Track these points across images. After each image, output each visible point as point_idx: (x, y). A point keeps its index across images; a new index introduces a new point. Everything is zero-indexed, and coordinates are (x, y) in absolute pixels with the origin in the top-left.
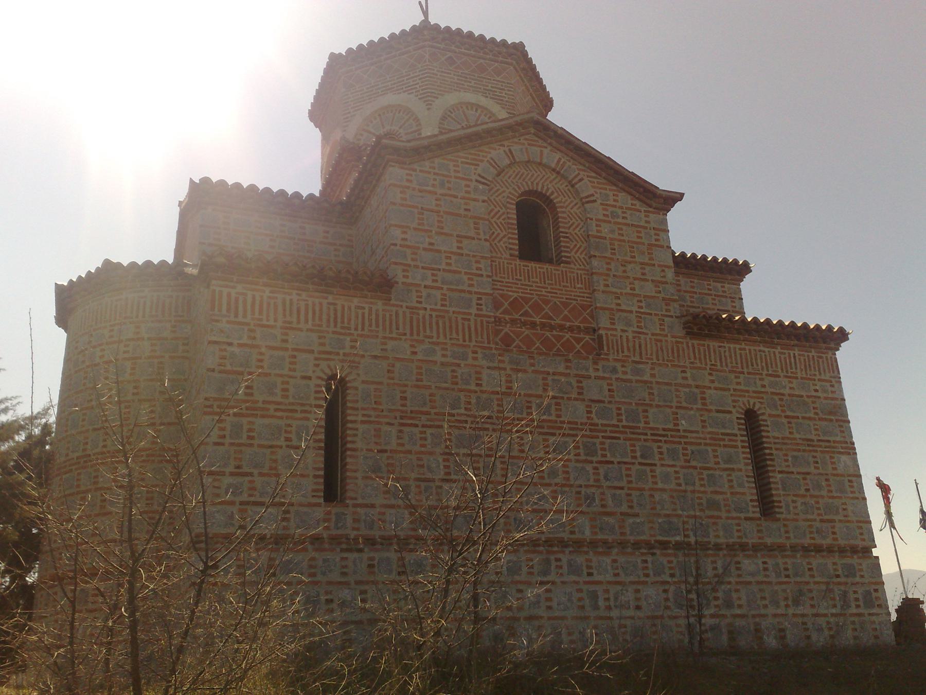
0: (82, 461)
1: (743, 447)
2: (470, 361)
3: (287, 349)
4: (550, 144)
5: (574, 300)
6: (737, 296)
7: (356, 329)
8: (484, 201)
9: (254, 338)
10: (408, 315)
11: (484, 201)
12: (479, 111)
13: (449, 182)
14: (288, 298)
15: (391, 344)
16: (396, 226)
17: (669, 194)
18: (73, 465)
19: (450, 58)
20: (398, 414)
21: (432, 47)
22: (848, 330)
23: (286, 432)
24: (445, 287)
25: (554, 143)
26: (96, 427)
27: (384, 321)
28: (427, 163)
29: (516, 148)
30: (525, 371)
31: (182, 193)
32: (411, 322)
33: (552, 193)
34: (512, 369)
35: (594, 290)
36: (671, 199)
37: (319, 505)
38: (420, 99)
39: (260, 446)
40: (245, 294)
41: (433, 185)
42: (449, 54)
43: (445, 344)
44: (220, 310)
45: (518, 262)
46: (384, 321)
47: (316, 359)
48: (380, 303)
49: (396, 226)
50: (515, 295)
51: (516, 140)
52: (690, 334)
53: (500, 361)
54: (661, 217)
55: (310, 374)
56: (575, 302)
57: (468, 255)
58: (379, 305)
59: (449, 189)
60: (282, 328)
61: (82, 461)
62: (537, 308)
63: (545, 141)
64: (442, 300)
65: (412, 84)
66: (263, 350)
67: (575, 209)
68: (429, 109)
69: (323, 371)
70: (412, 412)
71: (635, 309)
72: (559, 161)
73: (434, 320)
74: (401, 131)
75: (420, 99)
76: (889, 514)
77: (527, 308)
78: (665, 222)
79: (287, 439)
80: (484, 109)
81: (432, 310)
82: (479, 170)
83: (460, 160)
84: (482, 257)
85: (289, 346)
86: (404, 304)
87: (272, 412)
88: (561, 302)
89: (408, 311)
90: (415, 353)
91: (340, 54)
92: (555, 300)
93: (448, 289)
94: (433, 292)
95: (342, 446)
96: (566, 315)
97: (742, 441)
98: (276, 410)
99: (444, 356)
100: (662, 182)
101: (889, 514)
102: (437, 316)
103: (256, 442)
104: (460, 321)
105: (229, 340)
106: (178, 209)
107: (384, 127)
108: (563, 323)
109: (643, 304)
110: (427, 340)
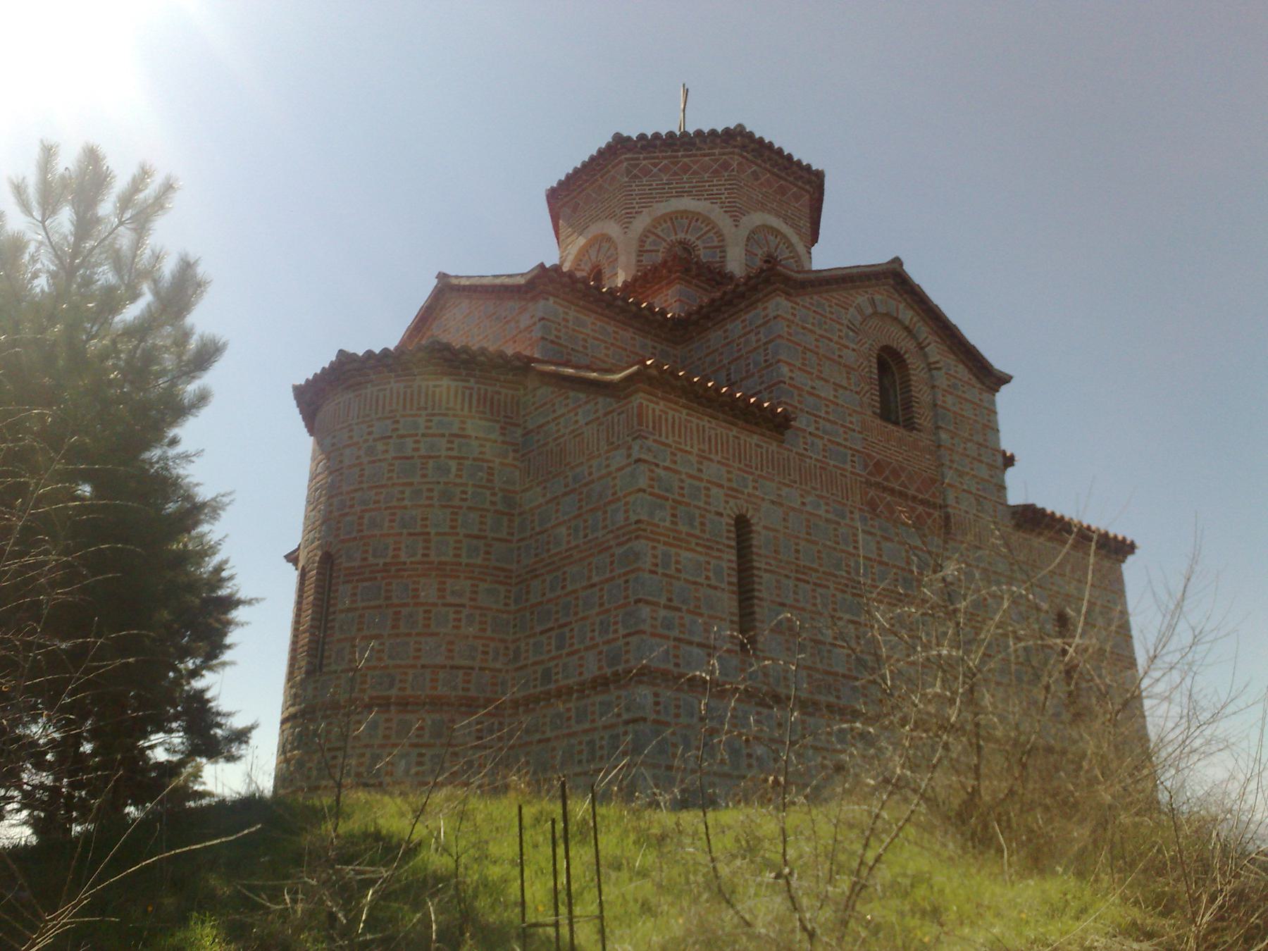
0: (393, 569)
2: (848, 521)
3: (701, 480)
4: (905, 300)
7: (756, 469)
8: (854, 350)
11: (854, 350)
12: (778, 239)
13: (825, 323)
14: (701, 423)
15: (785, 491)
16: (786, 362)
18: (379, 572)
19: (755, 171)
20: (793, 567)
21: (741, 155)
22: (1137, 543)
23: (706, 569)
24: (826, 437)
25: (909, 300)
26: (412, 531)
28: (808, 299)
29: (878, 297)
30: (892, 541)
33: (906, 352)
34: (882, 536)
35: (943, 465)
36: (1004, 379)
37: (736, 652)
38: (726, 212)
39: (687, 581)
40: (667, 413)
41: (813, 324)
42: (754, 168)
43: (828, 498)
44: (647, 427)
45: (878, 421)
47: (727, 495)
48: (775, 444)
49: (786, 362)
50: (878, 457)
51: (877, 289)
52: (1018, 526)
53: (872, 526)
54: (985, 396)
55: (721, 510)
57: (843, 406)
58: (774, 447)
59: (825, 330)
60: (697, 455)
61: (393, 569)
62: (896, 474)
63: (901, 295)
64: (824, 450)
65: (715, 192)
66: (684, 477)
67: (922, 374)
68: (736, 226)
69: (731, 509)
70: (804, 567)
72: (911, 320)
73: (818, 471)
74: (698, 242)
75: (726, 212)
76: (1261, 740)
78: (993, 403)
79: (708, 578)
80: (784, 237)
81: (816, 460)
82: (849, 317)
83: (834, 301)
84: (854, 411)
85: (705, 477)
86: (794, 450)
87: (693, 546)
89: (797, 457)
90: (803, 504)
91: (629, 138)
92: (910, 468)
93: (829, 440)
94: (817, 440)
98: (697, 544)
99: (827, 511)
100: (998, 361)
101: (1261, 740)
103: (683, 575)
105: (656, 461)
106: (435, 282)
107: (676, 234)
108: (916, 494)
110: (813, 492)
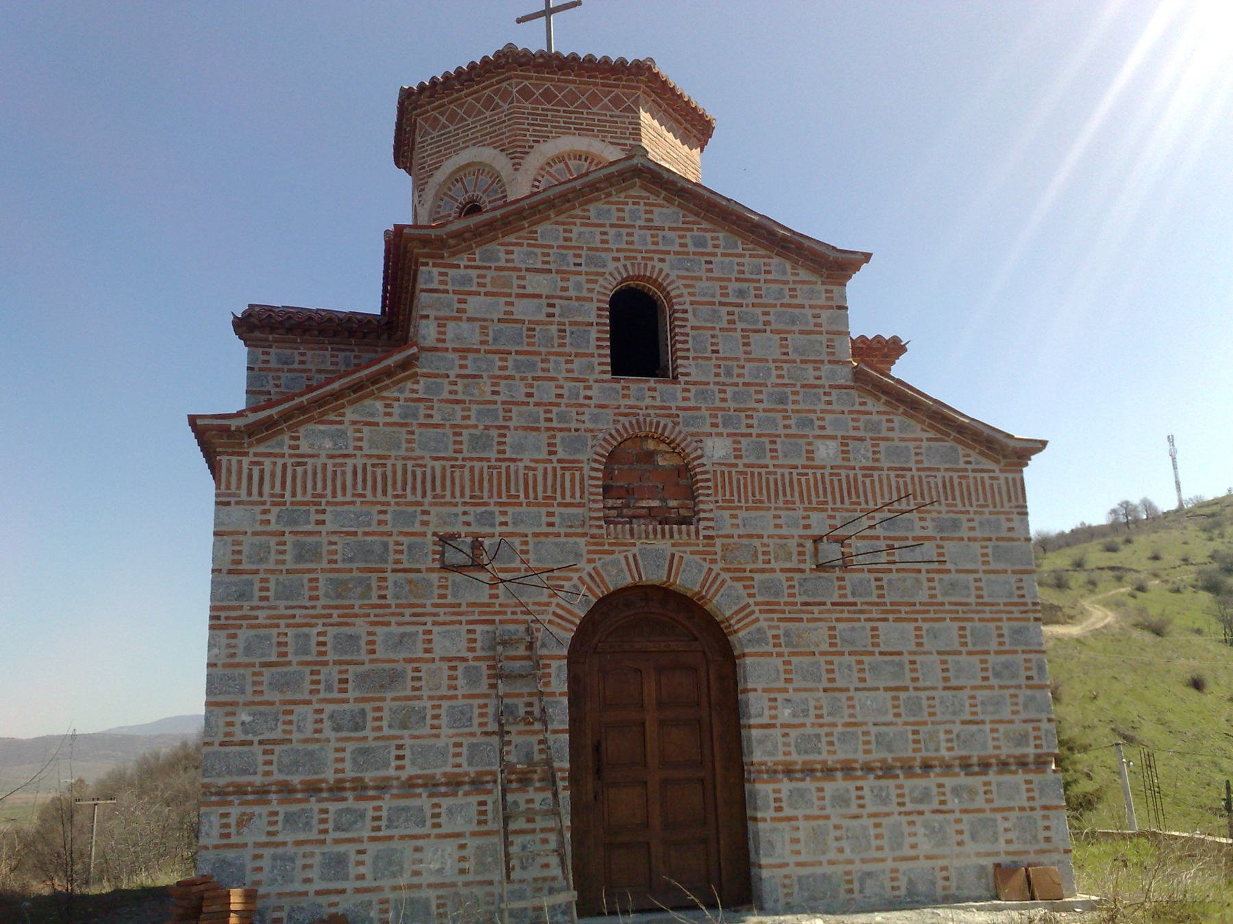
1: (681, 296)
5: (595, 114)
6: (219, 671)
9: (827, 662)
10: (486, 494)
17: (712, 196)
27: (364, 481)
31: (710, 114)
32: (250, 477)
46: (364, 481)
56: (594, 110)
71: (712, 379)
77: (479, 106)
88: (543, 104)
95: (673, 371)
96: (787, 404)
97: (681, 296)
102: (444, 496)
104: (958, 501)
109: (792, 422)
